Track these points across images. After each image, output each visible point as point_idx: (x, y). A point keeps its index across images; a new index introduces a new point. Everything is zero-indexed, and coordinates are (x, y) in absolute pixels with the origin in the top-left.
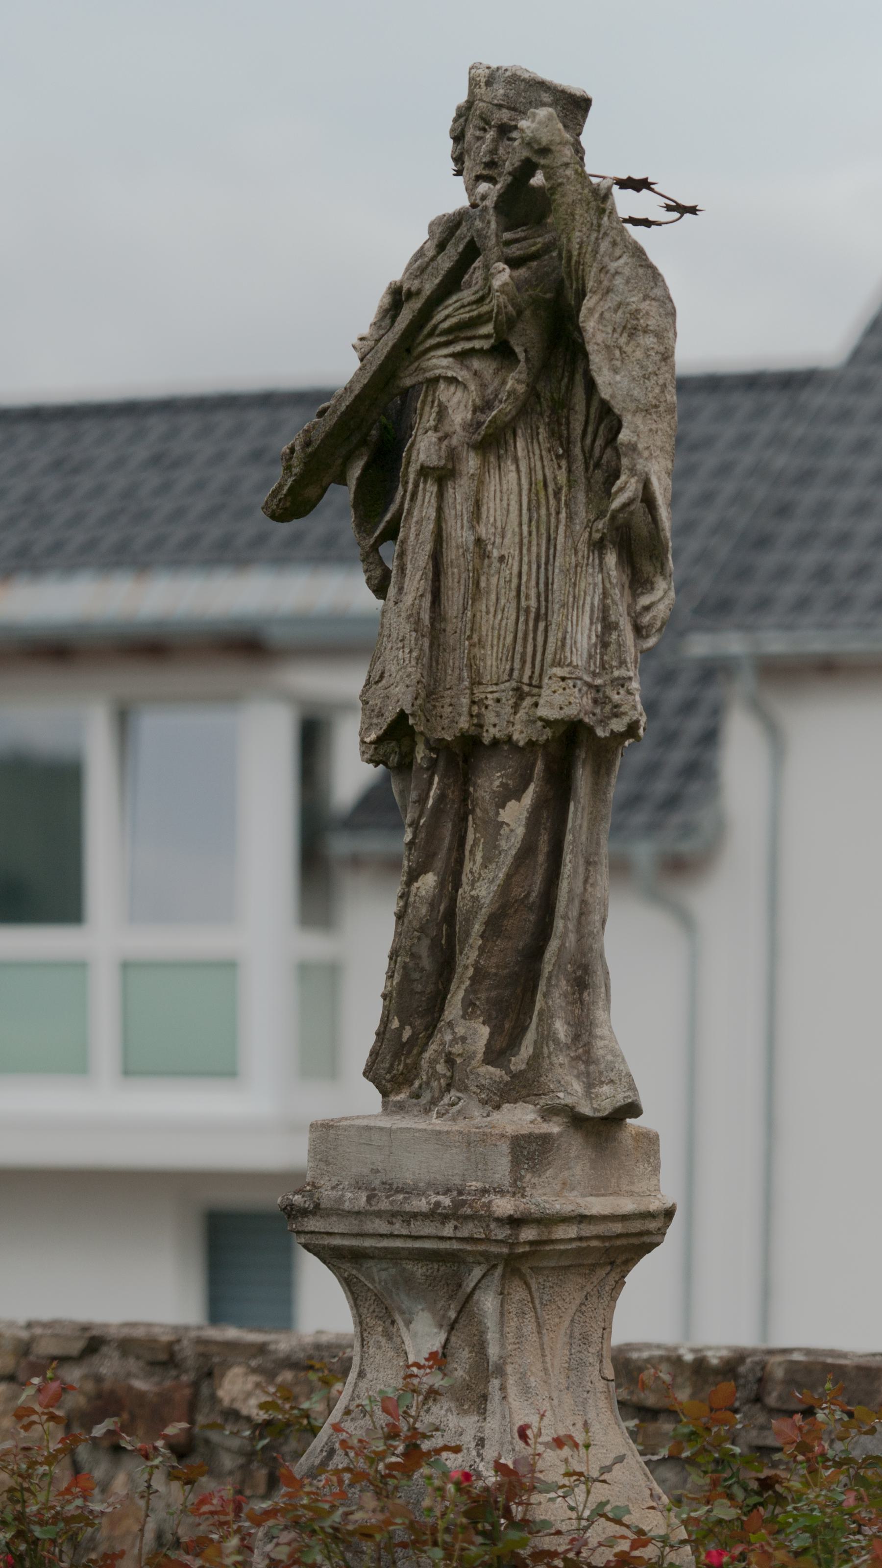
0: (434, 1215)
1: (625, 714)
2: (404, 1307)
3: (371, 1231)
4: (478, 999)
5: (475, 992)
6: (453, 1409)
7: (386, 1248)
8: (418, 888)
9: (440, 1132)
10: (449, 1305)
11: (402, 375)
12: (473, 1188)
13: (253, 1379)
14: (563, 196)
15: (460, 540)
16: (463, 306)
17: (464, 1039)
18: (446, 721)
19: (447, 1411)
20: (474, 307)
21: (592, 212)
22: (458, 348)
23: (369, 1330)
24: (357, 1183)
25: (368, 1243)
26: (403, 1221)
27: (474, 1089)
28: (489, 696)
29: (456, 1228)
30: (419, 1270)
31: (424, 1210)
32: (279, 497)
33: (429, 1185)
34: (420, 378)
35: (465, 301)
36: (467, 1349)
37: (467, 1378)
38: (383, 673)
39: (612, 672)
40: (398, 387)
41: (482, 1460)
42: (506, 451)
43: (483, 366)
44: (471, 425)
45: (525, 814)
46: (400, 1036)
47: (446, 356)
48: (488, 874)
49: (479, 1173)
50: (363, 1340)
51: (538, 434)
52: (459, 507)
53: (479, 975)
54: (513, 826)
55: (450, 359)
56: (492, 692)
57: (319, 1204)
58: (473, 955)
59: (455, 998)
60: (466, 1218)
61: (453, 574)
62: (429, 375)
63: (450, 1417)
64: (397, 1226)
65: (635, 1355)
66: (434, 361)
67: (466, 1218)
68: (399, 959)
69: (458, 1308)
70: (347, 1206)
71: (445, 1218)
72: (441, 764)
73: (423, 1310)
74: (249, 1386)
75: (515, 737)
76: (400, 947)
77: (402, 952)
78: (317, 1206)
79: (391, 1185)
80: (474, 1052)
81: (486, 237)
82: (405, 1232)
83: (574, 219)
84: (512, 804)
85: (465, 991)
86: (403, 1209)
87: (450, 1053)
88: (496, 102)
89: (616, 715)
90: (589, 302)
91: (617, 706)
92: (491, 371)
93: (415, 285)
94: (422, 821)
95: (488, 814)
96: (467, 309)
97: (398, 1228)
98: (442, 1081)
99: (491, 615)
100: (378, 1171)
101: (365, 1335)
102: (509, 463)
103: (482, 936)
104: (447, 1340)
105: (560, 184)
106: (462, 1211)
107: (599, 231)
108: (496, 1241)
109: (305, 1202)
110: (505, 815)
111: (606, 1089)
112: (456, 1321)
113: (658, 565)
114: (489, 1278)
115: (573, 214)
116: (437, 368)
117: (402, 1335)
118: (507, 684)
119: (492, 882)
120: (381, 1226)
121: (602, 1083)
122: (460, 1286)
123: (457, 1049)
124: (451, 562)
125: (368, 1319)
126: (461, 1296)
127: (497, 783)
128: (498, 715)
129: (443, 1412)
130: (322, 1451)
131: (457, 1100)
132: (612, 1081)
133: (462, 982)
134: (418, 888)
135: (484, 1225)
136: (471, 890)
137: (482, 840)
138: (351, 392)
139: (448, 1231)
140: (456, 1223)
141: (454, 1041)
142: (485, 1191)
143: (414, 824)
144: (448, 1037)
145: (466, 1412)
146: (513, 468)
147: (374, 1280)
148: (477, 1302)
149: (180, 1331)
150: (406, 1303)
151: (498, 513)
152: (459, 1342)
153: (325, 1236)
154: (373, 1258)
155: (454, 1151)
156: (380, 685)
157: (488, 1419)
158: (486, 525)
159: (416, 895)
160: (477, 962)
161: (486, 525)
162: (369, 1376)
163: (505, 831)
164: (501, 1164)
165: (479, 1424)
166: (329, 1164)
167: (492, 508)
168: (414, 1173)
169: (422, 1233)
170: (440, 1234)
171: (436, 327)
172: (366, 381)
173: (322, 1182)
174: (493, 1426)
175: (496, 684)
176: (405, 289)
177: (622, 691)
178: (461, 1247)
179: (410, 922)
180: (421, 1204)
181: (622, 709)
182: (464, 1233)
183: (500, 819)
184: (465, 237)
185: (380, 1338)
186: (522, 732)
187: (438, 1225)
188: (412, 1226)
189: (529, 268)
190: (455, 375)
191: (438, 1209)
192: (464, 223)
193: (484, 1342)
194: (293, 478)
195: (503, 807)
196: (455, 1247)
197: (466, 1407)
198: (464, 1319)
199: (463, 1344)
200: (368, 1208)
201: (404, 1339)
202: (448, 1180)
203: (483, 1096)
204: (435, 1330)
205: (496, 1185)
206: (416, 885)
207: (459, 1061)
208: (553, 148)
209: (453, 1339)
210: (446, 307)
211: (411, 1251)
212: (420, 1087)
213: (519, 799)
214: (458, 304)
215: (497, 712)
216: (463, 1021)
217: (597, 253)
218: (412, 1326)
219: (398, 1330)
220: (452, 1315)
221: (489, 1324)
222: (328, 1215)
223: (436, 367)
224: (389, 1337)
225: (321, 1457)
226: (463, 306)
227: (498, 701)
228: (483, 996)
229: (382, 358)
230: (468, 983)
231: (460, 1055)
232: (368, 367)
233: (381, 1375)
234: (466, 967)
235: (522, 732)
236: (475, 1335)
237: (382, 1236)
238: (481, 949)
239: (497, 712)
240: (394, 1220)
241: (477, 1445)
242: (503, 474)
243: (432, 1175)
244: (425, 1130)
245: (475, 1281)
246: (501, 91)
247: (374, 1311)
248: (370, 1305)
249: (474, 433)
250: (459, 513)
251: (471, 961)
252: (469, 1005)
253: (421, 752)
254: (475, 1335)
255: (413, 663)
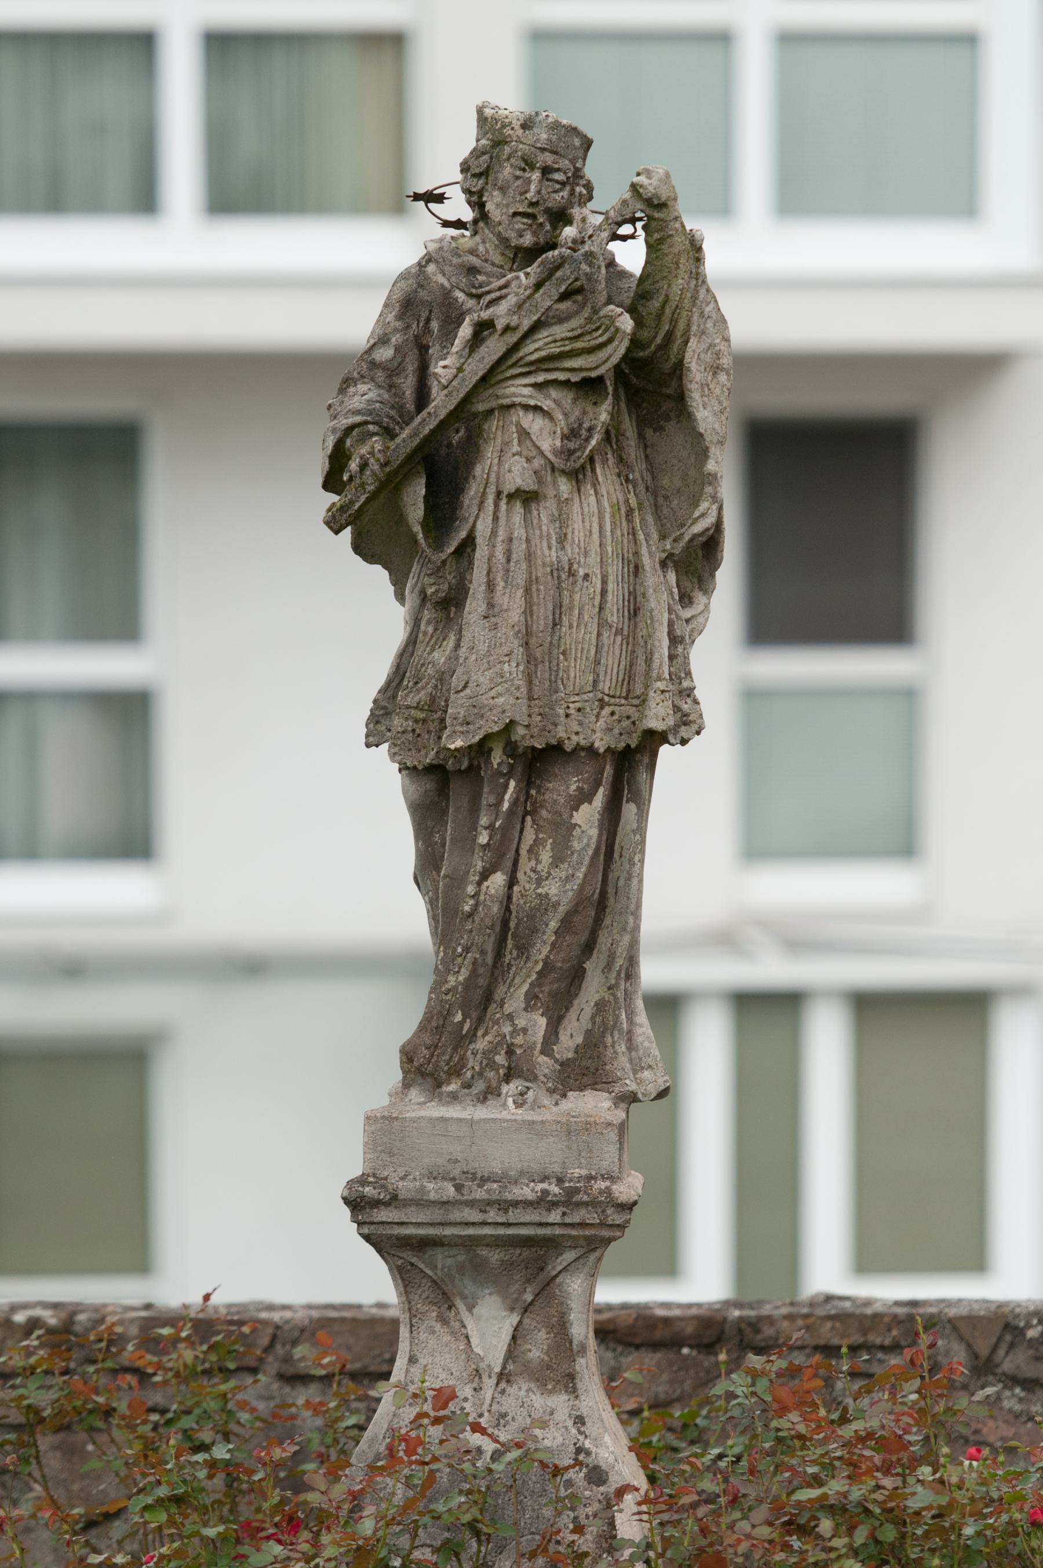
0: (544, 1202)
1: (694, 722)
2: (467, 1292)
3: (459, 1220)
4: (542, 992)
5: (540, 985)
6: (535, 1390)
7: (470, 1236)
8: (488, 887)
9: (533, 1122)
10: (525, 1289)
11: (475, 401)
12: (576, 1175)
14: (671, 246)
15: (548, 559)
16: (555, 341)
17: (525, 1030)
18: (536, 730)
19: (527, 1391)
20: (567, 342)
21: (691, 261)
22: (541, 378)
23: (419, 1316)
24: (431, 1173)
25: (448, 1231)
26: (499, 1209)
27: (542, 1078)
28: (571, 705)
29: (564, 1214)
30: (494, 1257)
31: (530, 1198)
32: (350, 512)
33: (522, 1173)
34: (494, 404)
35: (558, 337)
36: (543, 1330)
37: (546, 1358)
38: (467, 683)
39: (680, 683)
40: (469, 411)
41: (586, 1437)
42: (584, 475)
43: (561, 395)
44: (562, 452)
45: (597, 816)
46: (462, 1028)
47: (525, 386)
48: (562, 872)
49: (583, 1161)
50: (412, 1326)
51: (607, 459)
52: (544, 528)
54: (584, 828)
55: (530, 389)
56: (573, 702)
57: (397, 1195)
58: (545, 950)
59: (518, 992)
61: (538, 590)
62: (506, 401)
63: (533, 1397)
64: (492, 1214)
66: (513, 389)
68: (469, 955)
69: (537, 1291)
70: (433, 1196)
71: (554, 1204)
72: (519, 769)
73: (490, 1294)
75: (596, 745)
76: (472, 944)
77: (474, 949)
78: (395, 1197)
79: (474, 1174)
80: (535, 1043)
81: (596, 281)
82: (500, 1220)
83: (678, 268)
84: (585, 807)
85: (530, 984)
86: (504, 1198)
87: (512, 1044)
88: (539, 145)
89: (685, 724)
90: (693, 343)
91: (686, 715)
92: (569, 401)
93: (514, 320)
94: (498, 824)
95: (561, 816)
96: (558, 344)
97: (492, 1215)
98: (501, 1071)
99: (574, 630)
100: (457, 1161)
101: (414, 1321)
102: (589, 487)
103: (556, 933)
104: (520, 1322)
105: (671, 236)
106: (577, 1198)
107: (697, 279)
108: (611, 1226)
109: (379, 1193)
110: (579, 817)
111: (647, 1074)
112: (531, 1304)
113: (695, 580)
114: (582, 1261)
115: (677, 263)
116: (516, 396)
117: (464, 1319)
118: (591, 695)
119: (568, 879)
121: (643, 1068)
122: (542, 1269)
123: (519, 1040)
124: (537, 579)
125: (419, 1306)
127: (574, 787)
128: (580, 723)
129: (523, 1393)
130: (384, 1438)
131: (525, 1090)
132: (650, 1067)
133: (529, 976)
134: (488, 887)
135: (599, 1210)
136: (536, 888)
137: (551, 841)
138: (436, 416)
139: (555, 1217)
140: (565, 1209)
141: (515, 1032)
143: (490, 827)
144: (507, 1029)
145: (551, 1392)
146: (592, 492)
147: (436, 1267)
148: (561, 1284)
150: (469, 1287)
151: (582, 534)
152: (534, 1324)
153: (395, 1226)
154: (442, 1245)
155: (552, 1139)
156: (462, 694)
157: (583, 1398)
158: (572, 545)
159: (486, 893)
160: (547, 957)
161: (572, 545)
162: (422, 1361)
163: (577, 832)
164: (609, 1152)
165: (571, 1403)
166: (394, 1155)
167: (577, 528)
168: (502, 1162)
169: (522, 1220)
170: (544, 1221)
171: (522, 358)
172: (452, 407)
173: (386, 1174)
174: (590, 1404)
175: (577, 695)
176: (717, 348)
177: (689, 701)
178: (565, 1232)
179: (482, 920)
180: (526, 1192)
181: (691, 718)
182: (575, 1218)
183: (573, 821)
184: (568, 279)
185: (434, 1324)
186: (602, 739)
187: (544, 1212)
188: (510, 1213)
189: (574, 302)
190: (539, 404)
191: (547, 1196)
192: (567, 266)
193: (565, 1323)
194: (366, 495)
195: (577, 810)
196: (557, 1232)
197: (550, 1387)
198: (541, 1301)
199: (539, 1326)
200: (459, 1197)
201: (466, 1323)
202: (545, 1168)
203: (550, 1085)
204: (505, 1313)
205: (604, 1172)
206: (486, 884)
207: (519, 1051)
208: (669, 203)
209: (526, 1321)
210: (536, 341)
211: (497, 1237)
212: (473, 1077)
213: (590, 803)
214: (549, 339)
215: (579, 721)
216: (525, 1013)
217: (696, 299)
218: (475, 1311)
219: (457, 1313)
220: (529, 1297)
221: (573, 1305)
222: (405, 1206)
223: (515, 395)
224: (444, 1321)
225: (384, 1444)
226: (555, 341)
227: (579, 710)
228: (546, 989)
229: (471, 386)
230: (534, 977)
231: (521, 1046)
232: (455, 393)
233: (437, 1360)
234: (537, 962)
235: (602, 739)
236: (554, 1316)
237: (473, 1224)
238: (553, 945)
239: (579, 721)
240: (488, 1208)
241: (575, 1423)
242: (583, 497)
243: (526, 1164)
244: (515, 1120)
245: (565, 1264)
246: (544, 136)
247: (428, 1297)
248: (424, 1291)
249: (567, 460)
250: (545, 534)
251: (542, 956)
252: (531, 998)
253: (498, 757)
254: (554, 1316)
255: (520, 676)
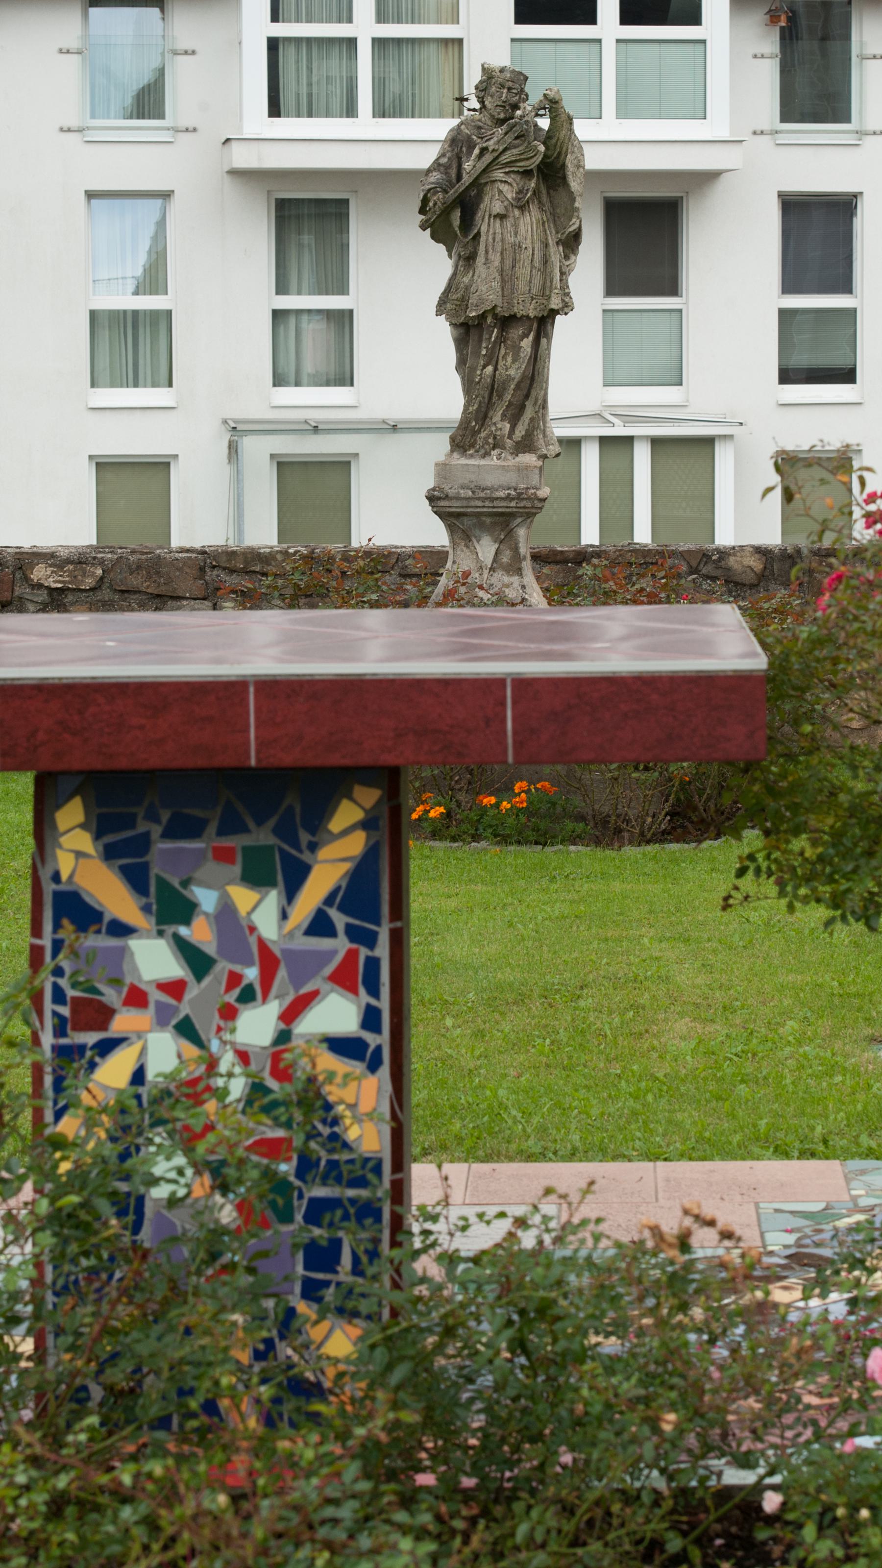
0: (508, 498)
13: (50, 569)
22: (507, 170)
25: (469, 510)
30: (488, 520)
53: (510, 403)
60: (523, 499)
65: (262, 551)
67: (523, 499)
74: (49, 573)
97: (487, 503)
110: (523, 344)
111: (551, 447)
120: (480, 504)
123: (498, 433)
126: (508, 529)
139: (513, 504)
141: (497, 430)
142: (527, 488)
143: (487, 347)
149: (646, 545)
150: (477, 532)
167: (522, 229)
180: (501, 494)
224: (467, 547)
